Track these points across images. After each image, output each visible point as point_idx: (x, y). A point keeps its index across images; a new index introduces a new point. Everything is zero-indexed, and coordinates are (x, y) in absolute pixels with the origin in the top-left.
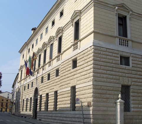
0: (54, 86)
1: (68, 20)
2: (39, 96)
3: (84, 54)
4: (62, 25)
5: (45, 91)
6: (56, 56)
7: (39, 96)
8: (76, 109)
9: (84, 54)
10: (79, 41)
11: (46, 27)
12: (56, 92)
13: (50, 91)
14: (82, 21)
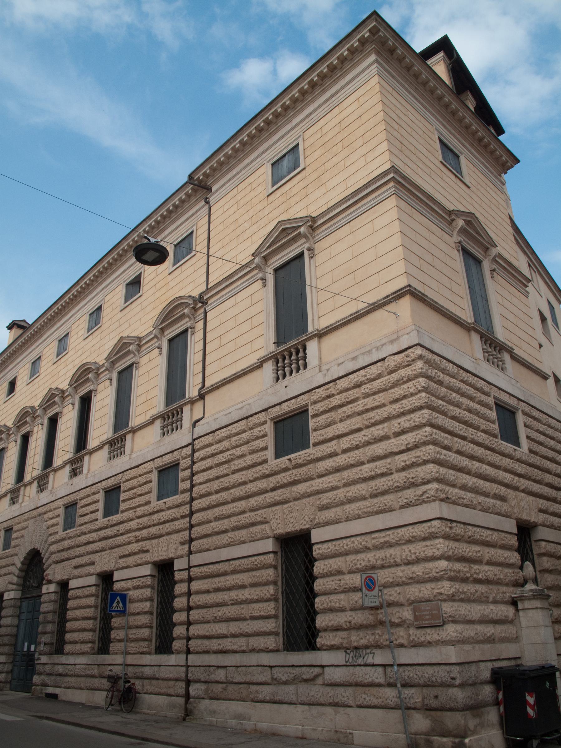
0: (97, 552)
1: (244, 257)
2: (49, 589)
3: (358, 386)
4: (191, 287)
5: (93, 563)
6: (104, 438)
7: (49, 589)
8: (319, 641)
9: (358, 386)
10: (185, 404)
11: (33, 357)
12: (165, 569)
13: (121, 561)
14: (141, 371)
